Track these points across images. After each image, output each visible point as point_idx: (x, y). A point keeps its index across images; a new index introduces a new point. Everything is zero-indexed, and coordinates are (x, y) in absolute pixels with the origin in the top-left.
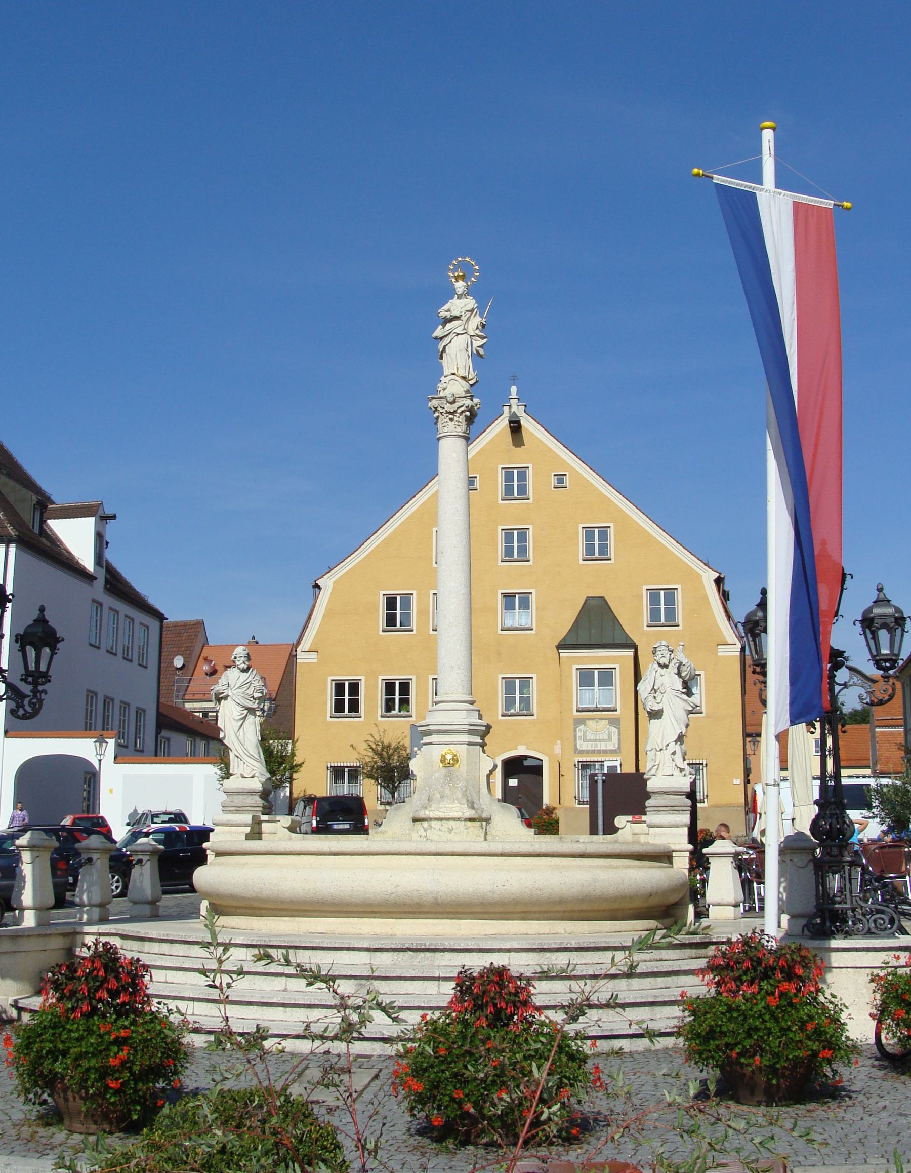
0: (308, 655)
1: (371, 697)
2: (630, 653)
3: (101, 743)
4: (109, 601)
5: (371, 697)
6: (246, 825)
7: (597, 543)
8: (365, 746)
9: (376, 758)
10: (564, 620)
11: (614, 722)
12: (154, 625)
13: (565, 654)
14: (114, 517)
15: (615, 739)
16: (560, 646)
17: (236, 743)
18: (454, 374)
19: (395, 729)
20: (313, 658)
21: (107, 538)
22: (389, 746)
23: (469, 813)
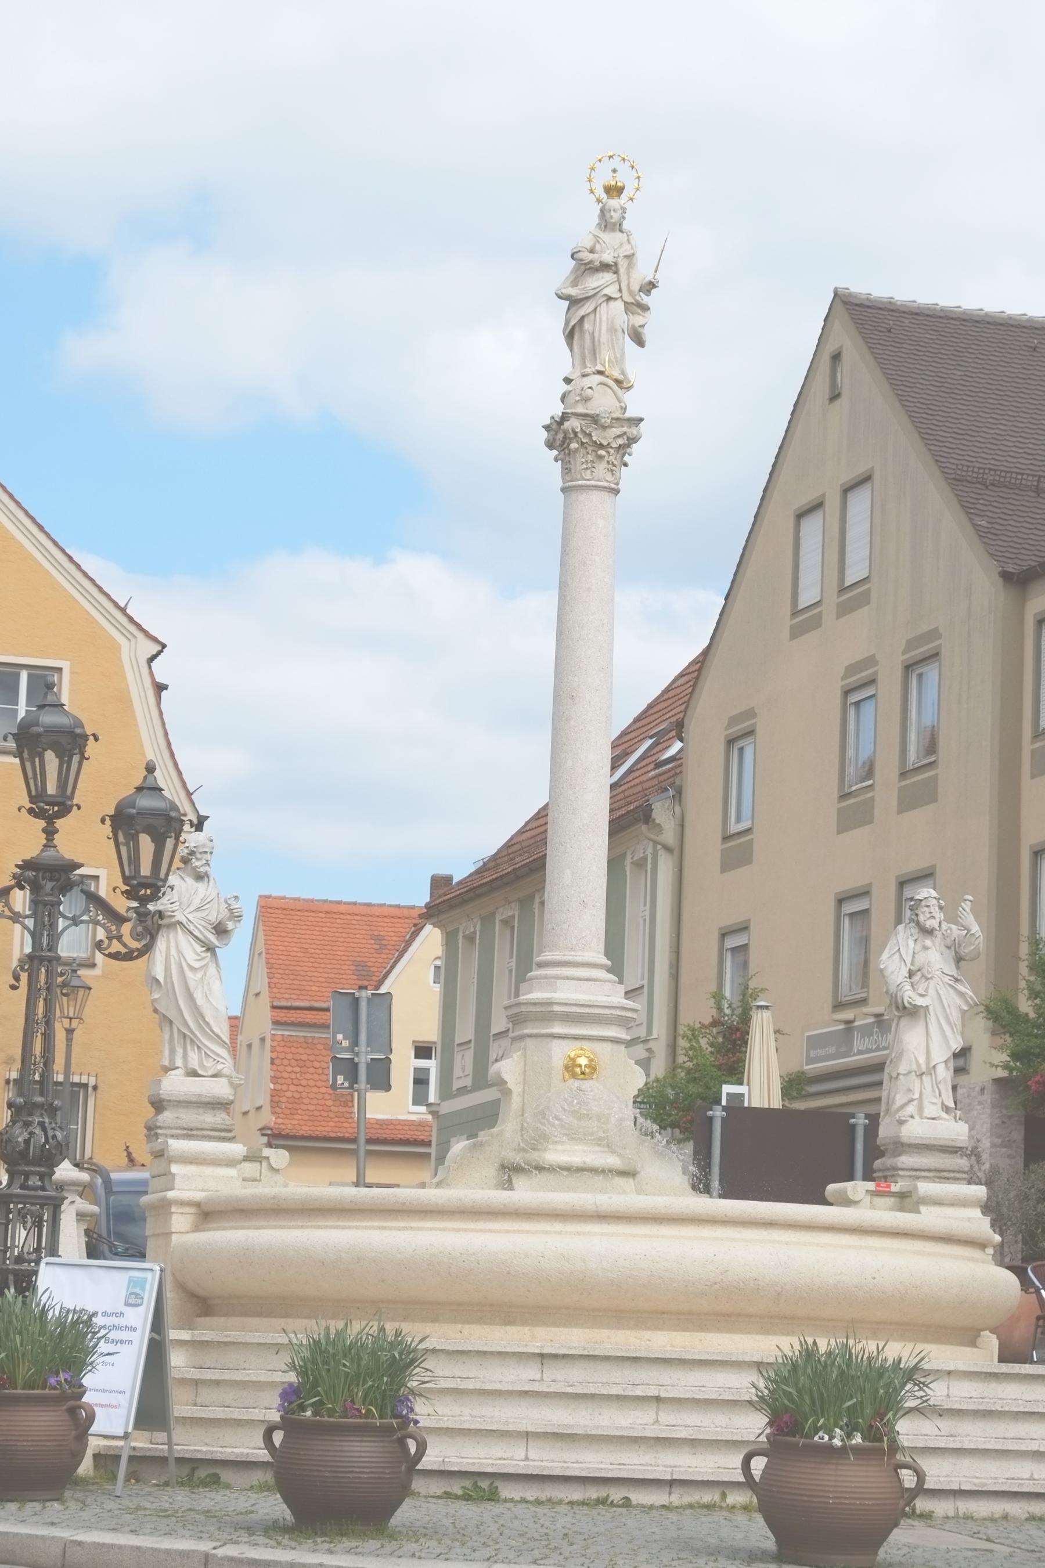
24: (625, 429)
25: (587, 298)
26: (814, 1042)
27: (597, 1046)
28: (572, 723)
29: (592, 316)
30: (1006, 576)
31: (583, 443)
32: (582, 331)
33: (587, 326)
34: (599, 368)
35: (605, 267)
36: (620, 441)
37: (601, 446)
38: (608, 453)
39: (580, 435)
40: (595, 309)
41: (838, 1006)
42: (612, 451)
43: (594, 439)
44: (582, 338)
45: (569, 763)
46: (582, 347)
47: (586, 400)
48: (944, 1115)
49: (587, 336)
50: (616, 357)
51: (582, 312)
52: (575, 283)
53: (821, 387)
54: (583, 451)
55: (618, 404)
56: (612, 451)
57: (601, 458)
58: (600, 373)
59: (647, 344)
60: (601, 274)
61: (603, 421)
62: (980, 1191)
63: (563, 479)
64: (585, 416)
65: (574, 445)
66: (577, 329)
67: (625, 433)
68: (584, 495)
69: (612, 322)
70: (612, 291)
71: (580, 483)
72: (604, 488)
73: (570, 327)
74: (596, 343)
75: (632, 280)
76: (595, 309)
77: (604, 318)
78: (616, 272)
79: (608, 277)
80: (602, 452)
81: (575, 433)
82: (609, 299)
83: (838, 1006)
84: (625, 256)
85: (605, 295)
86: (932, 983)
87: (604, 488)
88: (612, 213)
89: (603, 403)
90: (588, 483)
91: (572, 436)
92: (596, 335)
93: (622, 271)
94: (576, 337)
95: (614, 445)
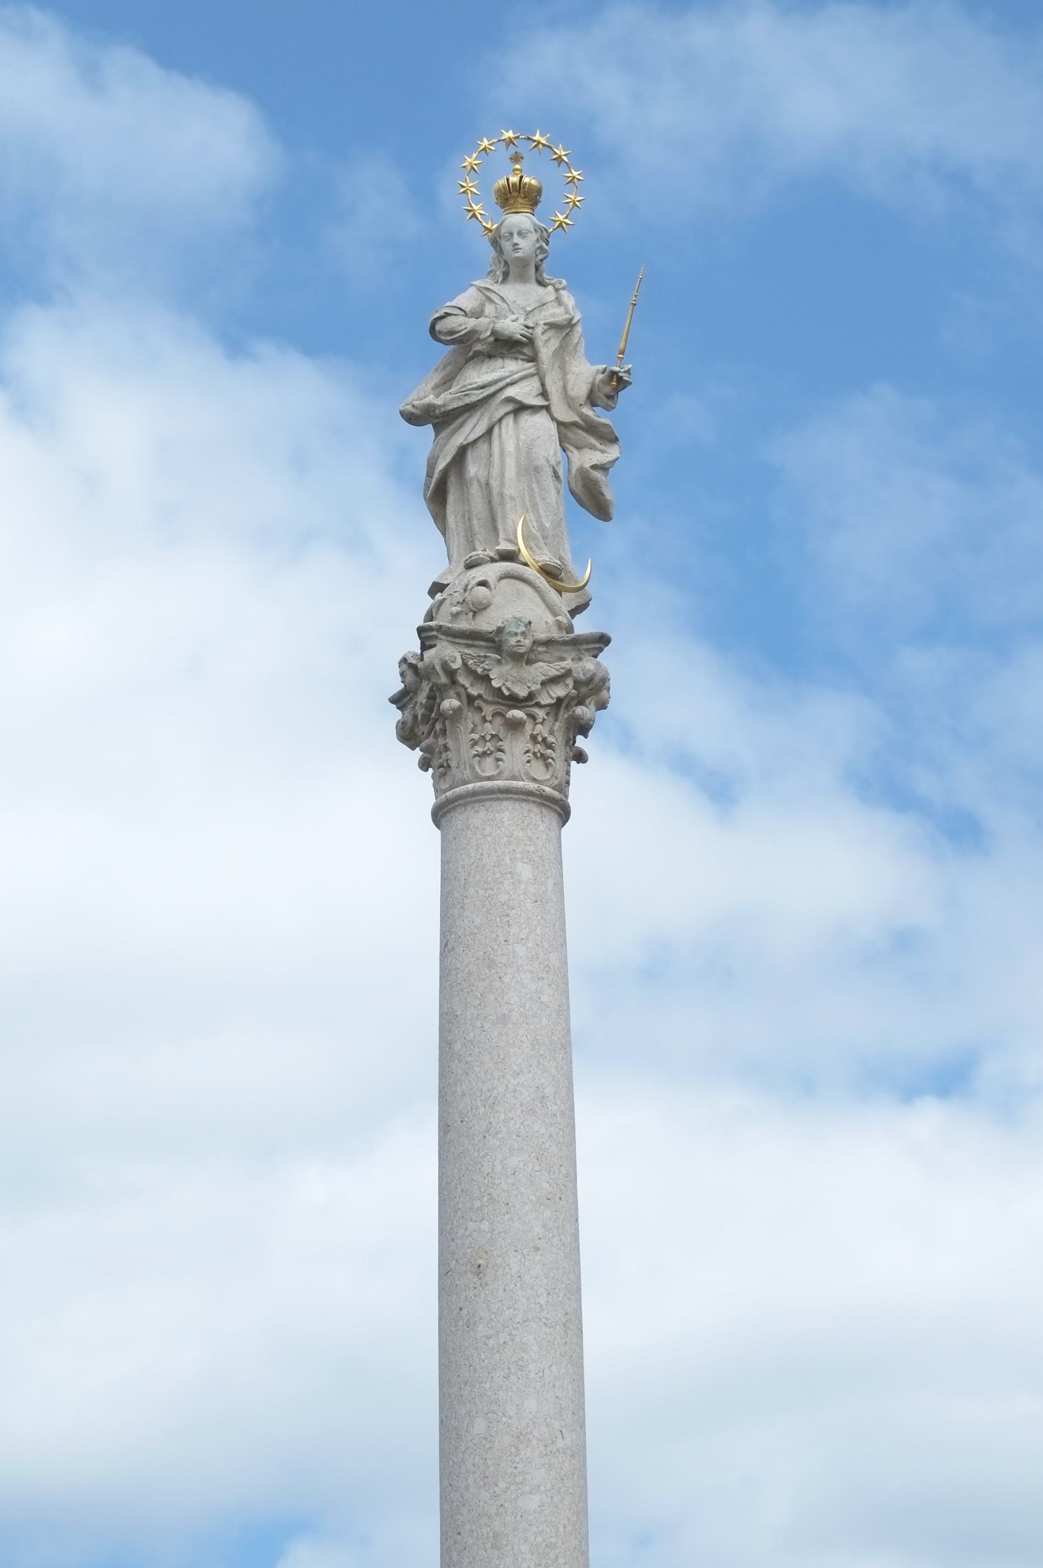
24: (567, 664)
25: (470, 408)
28: (481, 1330)
29: (483, 447)
31: (471, 699)
32: (463, 482)
33: (473, 468)
34: (504, 546)
35: (506, 346)
36: (559, 691)
37: (514, 701)
38: (532, 717)
39: (463, 679)
40: (489, 431)
42: (541, 713)
43: (495, 684)
44: (465, 498)
45: (480, 1426)
46: (467, 518)
47: (478, 609)
49: (475, 490)
50: (542, 528)
51: (460, 439)
52: (446, 383)
54: (471, 717)
55: (550, 619)
56: (541, 713)
57: (515, 726)
58: (509, 556)
59: (614, 511)
60: (499, 362)
61: (513, 641)
63: (436, 791)
64: (472, 637)
65: (450, 703)
66: (452, 480)
67: (568, 673)
68: (482, 814)
69: (528, 453)
70: (526, 392)
71: (470, 786)
72: (526, 795)
73: (436, 476)
74: (496, 499)
75: (571, 377)
76: (489, 431)
77: (510, 447)
78: (533, 359)
79: (510, 367)
80: (518, 714)
81: (451, 674)
82: (520, 408)
84: (552, 326)
85: (510, 400)
87: (526, 795)
88: (516, 239)
89: (520, 608)
90: (488, 784)
91: (444, 679)
92: (495, 484)
94: (451, 498)
95: (545, 700)
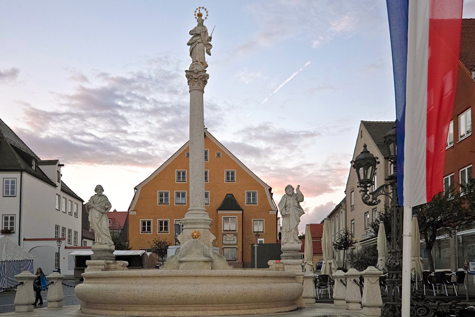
0: (133, 212)
1: (155, 226)
2: (241, 212)
3: (59, 242)
4: (63, 194)
5: (155, 226)
6: (102, 265)
7: (230, 176)
8: (153, 242)
9: (157, 246)
10: (220, 201)
11: (236, 235)
12: (80, 203)
13: (220, 212)
14: (63, 165)
15: (236, 240)
16: (217, 210)
17: (97, 228)
18: (197, 61)
19: (163, 236)
20: (135, 213)
21: (61, 173)
22: (161, 242)
23: (206, 259)
26: (363, 235)
27: (199, 230)
30: (385, 158)
41: (365, 230)
48: (295, 242)
53: (360, 136)
62: (47, 277)
70: (200, 41)
82: (199, 43)
83: (365, 230)
86: (291, 208)
93: (202, 35)
